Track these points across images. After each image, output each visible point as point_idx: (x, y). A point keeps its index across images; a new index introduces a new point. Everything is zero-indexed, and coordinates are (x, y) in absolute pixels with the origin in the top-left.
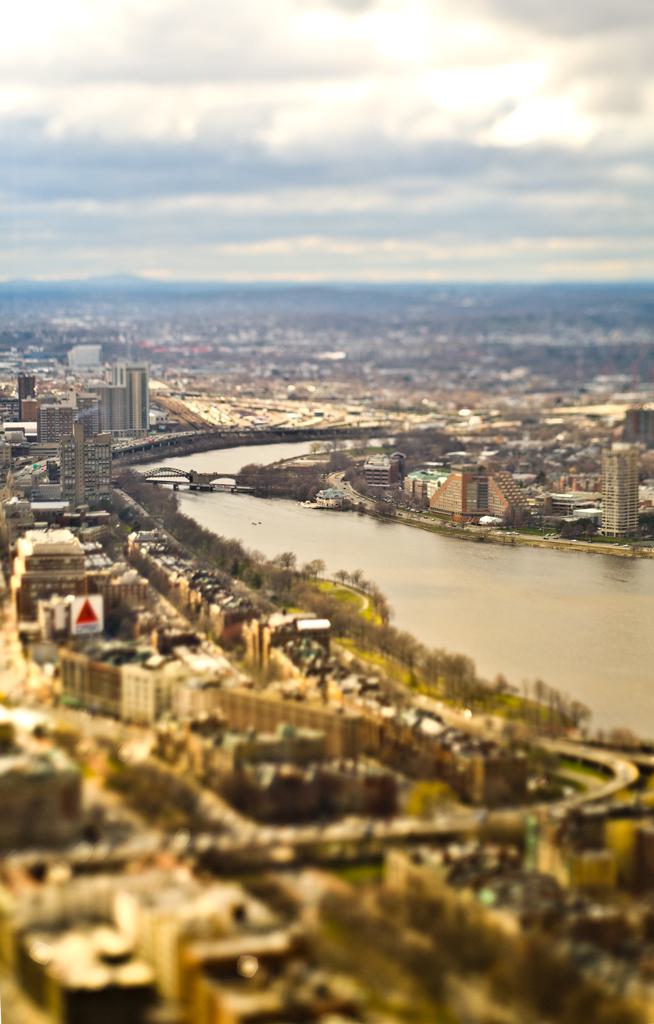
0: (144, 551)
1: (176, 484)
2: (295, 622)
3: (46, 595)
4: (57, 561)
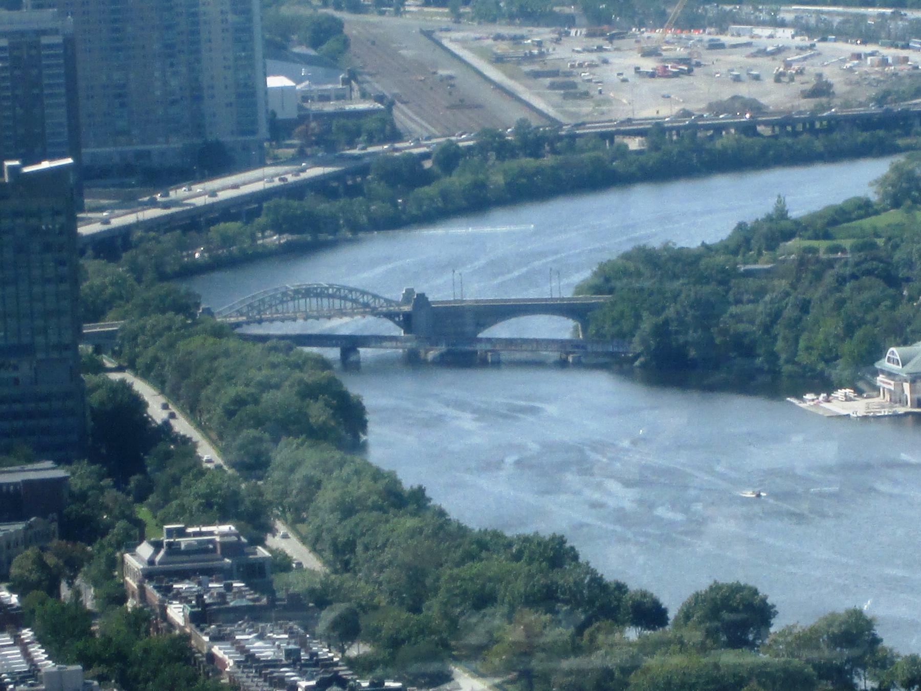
0: (177, 612)
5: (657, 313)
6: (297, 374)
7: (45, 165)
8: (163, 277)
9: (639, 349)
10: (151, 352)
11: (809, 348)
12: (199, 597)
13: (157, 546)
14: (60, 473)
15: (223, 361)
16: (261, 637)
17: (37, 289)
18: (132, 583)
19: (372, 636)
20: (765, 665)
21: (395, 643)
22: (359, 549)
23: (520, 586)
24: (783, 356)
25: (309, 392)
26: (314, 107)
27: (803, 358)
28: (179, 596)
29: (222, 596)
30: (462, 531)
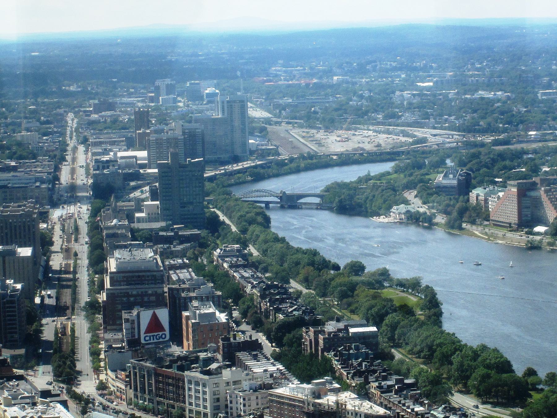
0: (226, 265)
1: (267, 203)
2: (346, 328)
3: (129, 307)
4: (130, 284)
6: (255, 210)
7: (197, 160)
8: (224, 187)
10: (221, 204)
11: (375, 206)
12: (231, 262)
13: (221, 250)
14: (199, 232)
16: (245, 271)
18: (215, 258)
19: (271, 272)
20: (363, 280)
21: (277, 273)
23: (306, 260)
25: (258, 214)
26: (260, 147)
27: (373, 208)
28: (226, 261)
29: (236, 262)
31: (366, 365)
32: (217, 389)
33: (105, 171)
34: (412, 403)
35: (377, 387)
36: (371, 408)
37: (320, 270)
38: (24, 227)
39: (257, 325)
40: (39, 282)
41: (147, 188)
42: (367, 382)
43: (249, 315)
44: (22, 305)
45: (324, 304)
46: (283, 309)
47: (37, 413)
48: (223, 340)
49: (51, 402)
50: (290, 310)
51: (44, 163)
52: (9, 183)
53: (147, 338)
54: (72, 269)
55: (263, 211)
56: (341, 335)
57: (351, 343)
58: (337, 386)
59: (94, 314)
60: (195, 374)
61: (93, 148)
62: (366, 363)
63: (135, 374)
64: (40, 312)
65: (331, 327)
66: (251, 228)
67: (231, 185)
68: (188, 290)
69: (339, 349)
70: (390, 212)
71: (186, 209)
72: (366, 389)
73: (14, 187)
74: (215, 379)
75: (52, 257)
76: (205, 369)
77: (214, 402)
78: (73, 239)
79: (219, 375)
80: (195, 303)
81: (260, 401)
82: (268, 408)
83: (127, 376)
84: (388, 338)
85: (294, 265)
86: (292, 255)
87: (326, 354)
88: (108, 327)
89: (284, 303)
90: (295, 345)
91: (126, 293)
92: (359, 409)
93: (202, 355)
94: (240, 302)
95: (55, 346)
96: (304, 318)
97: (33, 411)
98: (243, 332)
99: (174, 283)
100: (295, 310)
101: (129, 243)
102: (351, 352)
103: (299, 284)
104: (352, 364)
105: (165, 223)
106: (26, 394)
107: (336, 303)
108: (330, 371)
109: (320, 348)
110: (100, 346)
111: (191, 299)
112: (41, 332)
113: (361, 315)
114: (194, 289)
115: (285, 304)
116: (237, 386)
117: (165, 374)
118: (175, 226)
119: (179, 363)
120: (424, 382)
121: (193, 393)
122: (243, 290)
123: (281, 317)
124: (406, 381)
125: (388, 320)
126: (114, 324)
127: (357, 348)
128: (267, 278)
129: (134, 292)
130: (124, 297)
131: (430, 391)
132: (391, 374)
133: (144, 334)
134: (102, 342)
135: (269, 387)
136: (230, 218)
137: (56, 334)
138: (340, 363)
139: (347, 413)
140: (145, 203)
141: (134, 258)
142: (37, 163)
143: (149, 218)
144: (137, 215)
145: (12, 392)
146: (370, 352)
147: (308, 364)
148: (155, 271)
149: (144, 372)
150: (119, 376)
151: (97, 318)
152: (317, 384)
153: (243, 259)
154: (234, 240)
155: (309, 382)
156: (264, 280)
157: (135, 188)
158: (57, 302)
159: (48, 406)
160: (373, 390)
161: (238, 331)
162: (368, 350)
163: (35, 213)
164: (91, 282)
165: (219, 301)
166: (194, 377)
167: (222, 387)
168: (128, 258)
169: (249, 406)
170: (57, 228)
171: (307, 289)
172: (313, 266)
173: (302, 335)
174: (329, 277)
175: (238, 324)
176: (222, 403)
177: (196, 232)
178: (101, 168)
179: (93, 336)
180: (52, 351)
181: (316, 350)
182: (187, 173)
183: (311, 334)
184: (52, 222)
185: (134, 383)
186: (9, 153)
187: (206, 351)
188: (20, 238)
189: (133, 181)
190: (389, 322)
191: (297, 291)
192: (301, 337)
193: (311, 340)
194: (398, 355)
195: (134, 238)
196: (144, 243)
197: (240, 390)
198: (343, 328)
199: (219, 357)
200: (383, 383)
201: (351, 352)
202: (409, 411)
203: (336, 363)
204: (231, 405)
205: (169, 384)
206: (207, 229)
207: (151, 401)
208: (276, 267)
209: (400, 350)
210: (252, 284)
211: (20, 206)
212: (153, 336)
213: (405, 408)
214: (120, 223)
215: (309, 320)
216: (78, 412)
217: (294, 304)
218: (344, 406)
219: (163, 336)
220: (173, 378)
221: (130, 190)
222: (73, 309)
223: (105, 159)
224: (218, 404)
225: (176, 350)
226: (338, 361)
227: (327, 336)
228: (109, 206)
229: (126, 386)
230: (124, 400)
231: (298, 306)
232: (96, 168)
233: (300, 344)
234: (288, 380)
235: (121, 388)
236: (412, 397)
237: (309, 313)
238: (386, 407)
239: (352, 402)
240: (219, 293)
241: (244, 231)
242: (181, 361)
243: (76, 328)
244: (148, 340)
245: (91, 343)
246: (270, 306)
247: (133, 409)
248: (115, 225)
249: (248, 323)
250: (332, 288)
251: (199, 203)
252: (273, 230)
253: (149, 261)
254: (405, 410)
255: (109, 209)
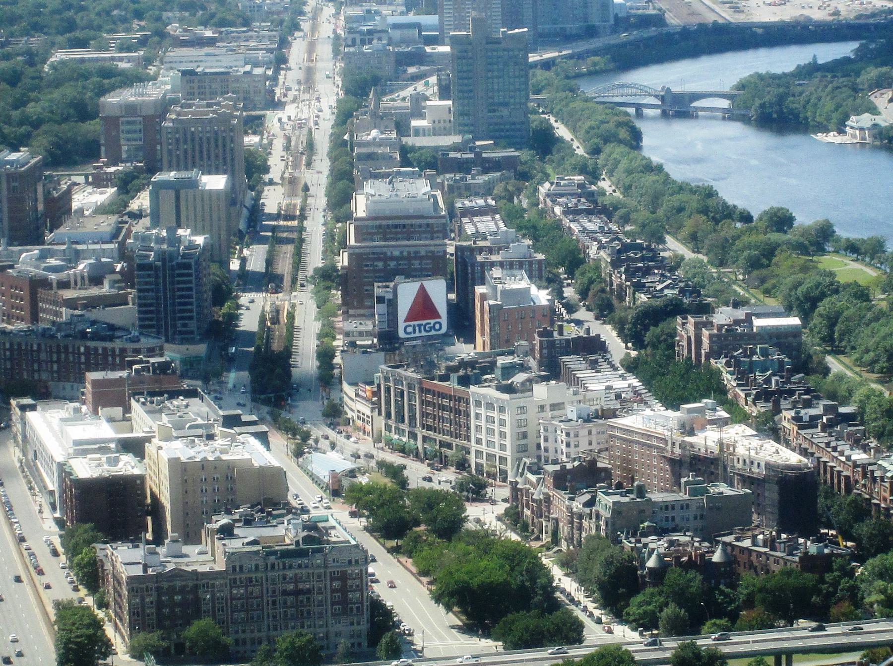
0: (558, 210)
1: (639, 108)
2: (748, 319)
3: (388, 276)
5: (760, 99)
6: (616, 118)
7: (517, 31)
8: (567, 77)
9: (753, 113)
10: (559, 107)
11: (820, 115)
12: (567, 204)
13: (552, 184)
14: (517, 154)
15: (586, 111)
16: (590, 221)
17: (512, 80)
18: (541, 198)
19: (635, 222)
20: (790, 239)
21: (644, 226)
22: (633, 188)
23: (695, 205)
24: (810, 118)
25: (619, 125)
26: (633, 12)
27: (818, 119)
28: (559, 204)
29: (576, 204)
30: (674, 182)
31: (777, 381)
32: (524, 416)
33: (366, 49)
34: (848, 447)
35: (793, 418)
36: (777, 452)
37: (717, 222)
38: (216, 140)
39: (604, 311)
40: (241, 235)
41: (433, 80)
42: (777, 410)
43: (591, 293)
44: (204, 272)
45: (719, 278)
46: (647, 285)
47: (212, 452)
48: (541, 335)
49: (240, 434)
50: (658, 288)
51: (262, 33)
52: (198, 66)
53: (410, 329)
54: (298, 213)
55: (630, 121)
56: (739, 330)
57: (755, 345)
58: (723, 414)
59: (328, 288)
60: (486, 391)
61: (347, 9)
62: (777, 378)
63: (388, 390)
64: (238, 285)
65: (723, 316)
66: (608, 149)
67: (579, 76)
68: (490, 250)
69: (735, 354)
70: (846, 126)
71: (497, 114)
72: (774, 422)
73: (206, 74)
74: (519, 400)
75: (265, 193)
76: (504, 383)
77: (518, 439)
78: (304, 162)
79: (527, 394)
80: (497, 272)
81: (594, 438)
82: (607, 449)
83: (374, 394)
84: (821, 339)
85: (674, 211)
86: (672, 195)
87: (712, 361)
88: (351, 312)
89: (650, 275)
90: (663, 346)
91: (382, 254)
92: (757, 453)
93: (501, 361)
94: (577, 273)
95: (258, 342)
96: (681, 300)
97: (206, 448)
98: (579, 323)
99: (468, 238)
100: (667, 287)
101: (395, 169)
102: (755, 358)
103: (683, 243)
104: (755, 379)
105: (460, 137)
106: (200, 421)
107: (741, 277)
108: (719, 392)
109: (703, 352)
110: (335, 343)
111: (492, 264)
112: (237, 317)
113: (780, 298)
114: (500, 249)
115: (652, 277)
116: (556, 413)
117: (437, 390)
118: (478, 143)
119: (462, 372)
120: (875, 412)
121: (483, 423)
122: (585, 252)
123: (643, 298)
124: (842, 410)
125: (823, 307)
126: (361, 306)
127: (765, 353)
128: (626, 234)
129: (396, 253)
130: (379, 259)
131: (884, 427)
132: (818, 398)
133: (406, 321)
134: (338, 337)
135: (613, 414)
136: (574, 130)
137: (263, 320)
138: (735, 377)
139: (736, 461)
140: (428, 103)
141: (397, 195)
142: (250, 33)
143: (434, 128)
144: (415, 123)
145: (176, 418)
146: (786, 360)
147: (682, 376)
148: (431, 218)
149: (403, 385)
150: (361, 393)
151: (334, 295)
152: (689, 411)
153: (590, 202)
154: (575, 168)
155: (677, 408)
156: (621, 236)
157: (415, 78)
158: (267, 268)
159: (233, 440)
160: (785, 424)
161: (569, 322)
162: (782, 357)
163: (236, 117)
164: (329, 236)
165: (540, 270)
166: (484, 396)
167: (532, 414)
168: (387, 195)
169: (577, 446)
170: (278, 145)
171: (694, 252)
172: (707, 215)
173: (675, 329)
174: (732, 233)
175: (571, 308)
176: (531, 441)
177: (511, 152)
178: (358, 41)
179: (323, 325)
180: (252, 349)
181: (698, 355)
182: (501, 53)
183: (691, 327)
184: (269, 133)
185: (386, 404)
186: (203, 15)
187: (511, 353)
188: (209, 158)
189: (412, 65)
190: (825, 310)
191: (676, 256)
192: (673, 334)
193: (689, 338)
194: (835, 365)
195: (406, 162)
196: (421, 170)
197: (563, 418)
198: (743, 317)
199: (533, 363)
200: (803, 412)
201: (755, 358)
202: (843, 459)
203: (729, 376)
204: (547, 444)
205: (444, 408)
206: (532, 148)
207: (414, 436)
208: (643, 214)
209: (842, 357)
210: (600, 242)
211: (209, 105)
212: (419, 326)
213: (836, 454)
214: (383, 136)
215: (690, 305)
216: (289, 453)
217: (665, 277)
218: (731, 449)
219: (437, 327)
220: (450, 398)
221: (408, 80)
222: (294, 280)
223: (365, 28)
224: (524, 442)
225: (463, 351)
226: (732, 373)
227: (715, 331)
228: (366, 106)
229: (372, 410)
230: (368, 434)
231: (674, 280)
232: (350, 43)
233: (672, 346)
234: (646, 403)
235: (363, 414)
236: (850, 435)
237: (692, 293)
238: (804, 452)
239: (746, 443)
240: (540, 256)
241: (596, 151)
242: (466, 369)
243: (296, 314)
244: (410, 333)
245: (320, 336)
246: (626, 280)
247: (382, 449)
248: (374, 139)
249: (589, 309)
250: (736, 252)
251: (521, 104)
252: (646, 153)
253: (422, 200)
254: (836, 458)
255: (366, 112)
